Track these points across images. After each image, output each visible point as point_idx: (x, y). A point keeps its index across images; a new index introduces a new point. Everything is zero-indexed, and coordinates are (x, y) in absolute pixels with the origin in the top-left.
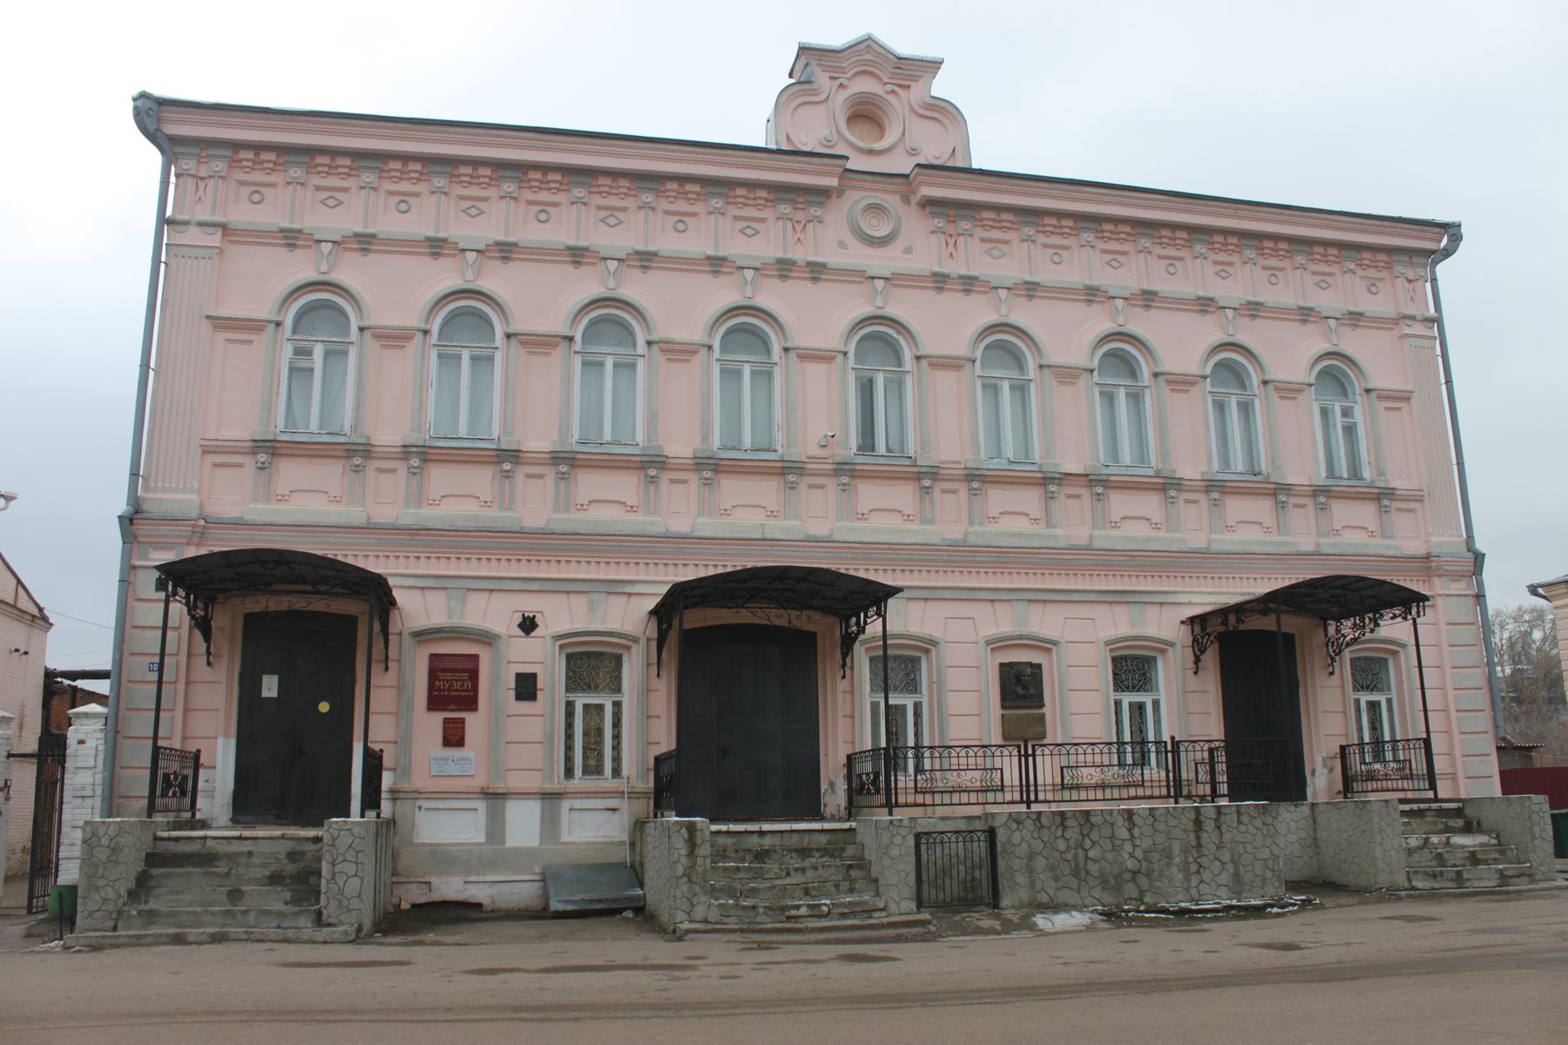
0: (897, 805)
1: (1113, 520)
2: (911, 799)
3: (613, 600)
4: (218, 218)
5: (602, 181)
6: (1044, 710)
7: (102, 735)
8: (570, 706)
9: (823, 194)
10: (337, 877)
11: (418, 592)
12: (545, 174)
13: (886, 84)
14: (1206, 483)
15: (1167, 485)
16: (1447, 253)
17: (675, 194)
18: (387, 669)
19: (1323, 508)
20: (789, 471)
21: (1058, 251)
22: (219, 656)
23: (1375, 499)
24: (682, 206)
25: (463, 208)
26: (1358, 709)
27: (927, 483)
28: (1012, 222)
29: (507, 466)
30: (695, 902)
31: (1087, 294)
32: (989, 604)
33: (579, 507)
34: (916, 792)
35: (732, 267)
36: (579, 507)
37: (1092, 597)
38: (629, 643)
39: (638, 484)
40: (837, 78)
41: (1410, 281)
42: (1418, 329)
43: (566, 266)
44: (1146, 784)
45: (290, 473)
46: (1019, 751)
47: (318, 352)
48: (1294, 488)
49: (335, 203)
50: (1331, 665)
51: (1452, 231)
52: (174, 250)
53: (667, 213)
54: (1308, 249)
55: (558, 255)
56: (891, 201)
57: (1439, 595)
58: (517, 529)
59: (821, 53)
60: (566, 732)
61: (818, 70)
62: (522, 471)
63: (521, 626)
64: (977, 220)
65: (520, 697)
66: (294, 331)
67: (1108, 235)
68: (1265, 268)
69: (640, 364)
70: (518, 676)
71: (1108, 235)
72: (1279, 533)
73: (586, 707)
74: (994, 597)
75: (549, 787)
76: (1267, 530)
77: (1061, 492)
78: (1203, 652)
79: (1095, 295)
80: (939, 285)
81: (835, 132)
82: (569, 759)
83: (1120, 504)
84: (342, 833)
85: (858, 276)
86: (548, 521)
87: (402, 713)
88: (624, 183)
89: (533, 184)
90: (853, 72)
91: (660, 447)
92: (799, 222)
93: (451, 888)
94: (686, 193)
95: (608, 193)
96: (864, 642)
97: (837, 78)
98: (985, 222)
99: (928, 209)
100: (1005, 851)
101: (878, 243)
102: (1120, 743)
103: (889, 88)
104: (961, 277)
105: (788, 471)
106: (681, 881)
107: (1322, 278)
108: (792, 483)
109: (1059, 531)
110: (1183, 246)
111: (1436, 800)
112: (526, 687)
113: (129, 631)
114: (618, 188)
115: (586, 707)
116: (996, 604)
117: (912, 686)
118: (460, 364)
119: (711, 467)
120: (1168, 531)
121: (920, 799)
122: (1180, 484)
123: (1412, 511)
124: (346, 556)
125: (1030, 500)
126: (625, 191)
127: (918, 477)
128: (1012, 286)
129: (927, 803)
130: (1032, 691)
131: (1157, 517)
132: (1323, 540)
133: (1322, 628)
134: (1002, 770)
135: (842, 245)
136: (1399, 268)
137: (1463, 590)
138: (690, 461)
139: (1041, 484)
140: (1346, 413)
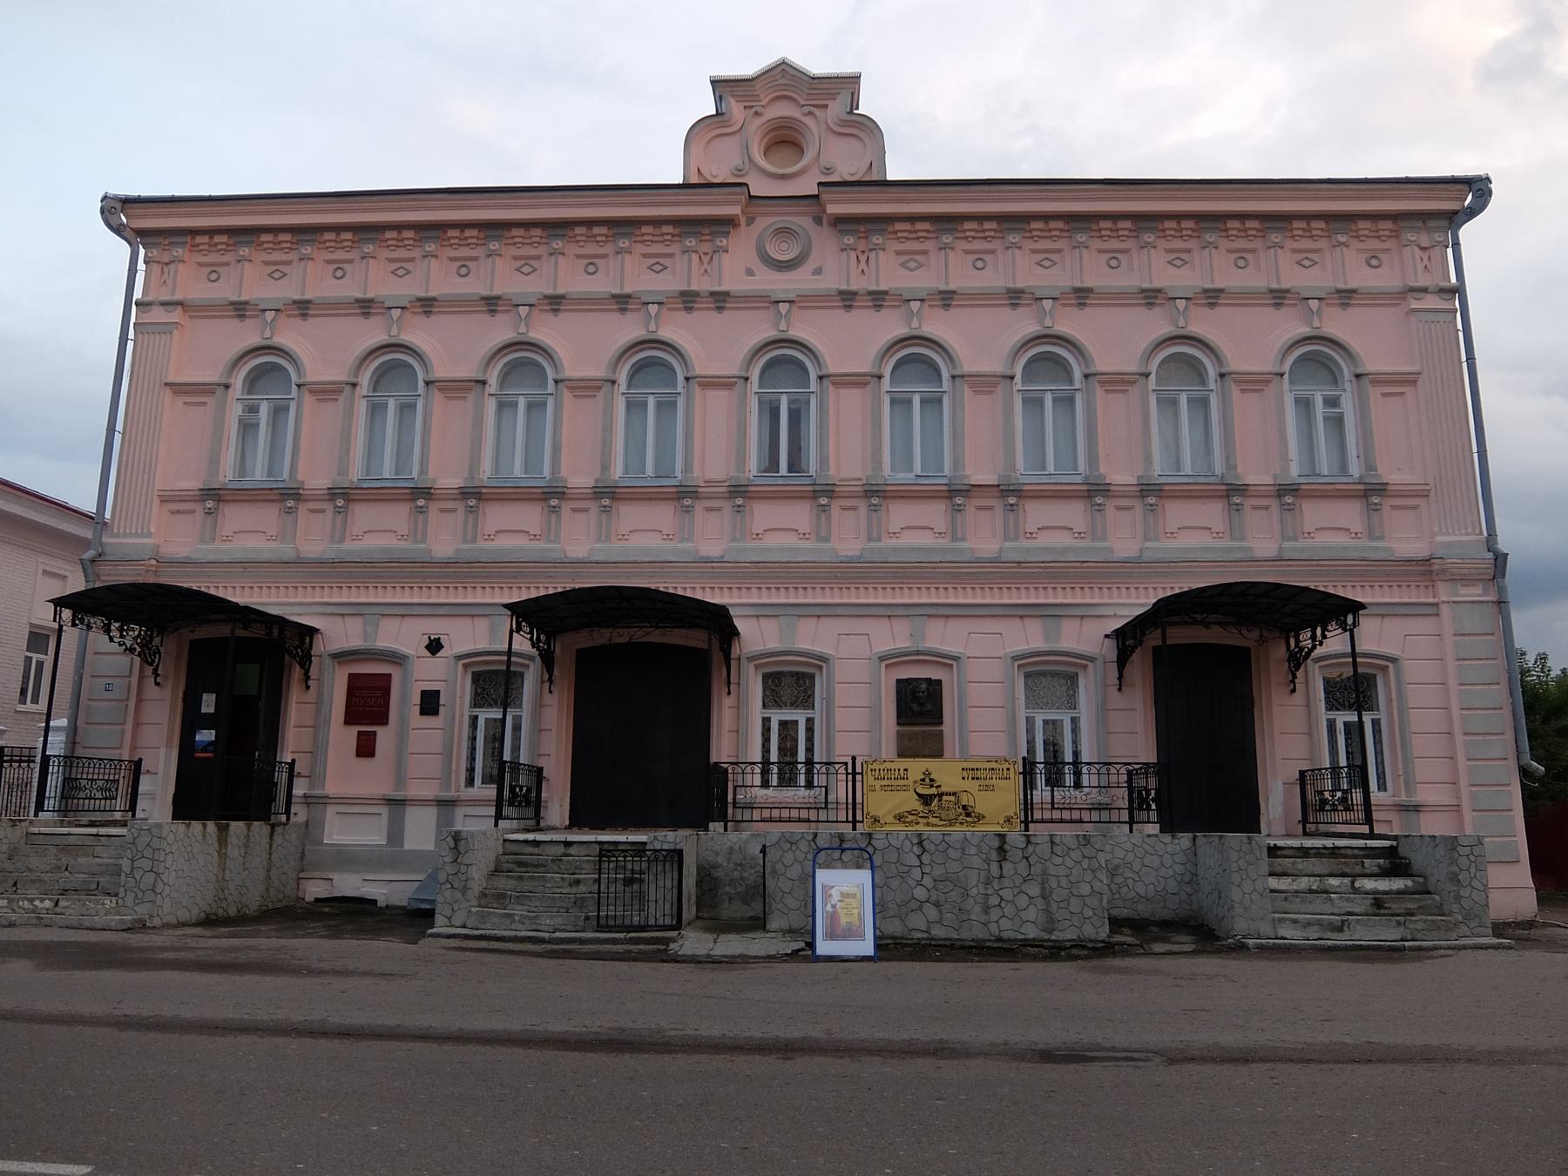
0: (1032, 822)
1: (754, 531)
2: (1047, 815)
3: (804, 621)
4: (178, 297)
5: (515, 232)
6: (942, 728)
7: (63, 746)
8: (474, 719)
9: (729, 223)
10: (135, 872)
11: (340, 619)
12: (1046, 223)
13: (803, 106)
14: (1140, 488)
15: (1094, 492)
16: (1472, 212)
17: (584, 238)
18: (308, 687)
19: (606, 510)
20: (683, 495)
21: (1115, 255)
22: (166, 678)
23: (1224, 497)
24: (591, 249)
25: (649, 264)
26: (766, 730)
27: (1012, 500)
28: (928, 231)
29: (421, 503)
30: (456, 908)
31: (1011, 298)
32: (887, 620)
33: (486, 537)
34: (1053, 808)
35: (637, 304)
36: (486, 537)
37: (999, 611)
38: (527, 662)
39: (811, 511)
40: (752, 107)
41: (1424, 249)
42: (1432, 302)
43: (1203, 308)
44: (829, 806)
45: (235, 517)
46: (846, 769)
47: (264, 409)
48: (1250, 488)
49: (660, 268)
50: (1293, 681)
51: (1477, 189)
52: (137, 327)
53: (1100, 251)
54: (1221, 225)
55: (222, 311)
56: (803, 222)
57: (1443, 602)
58: (428, 560)
59: (733, 84)
60: (813, 745)
61: (732, 101)
62: (434, 507)
63: (427, 647)
64: (1026, 231)
65: (423, 712)
66: (629, 385)
67: (1038, 233)
68: (967, 252)
69: (1078, 398)
70: (423, 692)
71: (1038, 233)
72: (1232, 539)
73: (1046, 722)
74: (889, 612)
75: (445, 795)
76: (1218, 535)
77: (970, 507)
78: (1297, 669)
79: (1019, 298)
80: (847, 303)
81: (747, 160)
82: (471, 770)
83: (1036, 514)
84: (142, 832)
85: (762, 302)
86: (1141, 550)
87: (318, 727)
88: (537, 232)
89: (452, 241)
90: (770, 97)
91: (1237, 477)
92: (706, 254)
93: (349, 884)
94: (595, 236)
95: (539, 243)
96: (1319, 659)
97: (752, 107)
98: (899, 235)
99: (840, 227)
100: (774, 871)
101: (786, 267)
102: (766, 763)
103: (806, 109)
104: (870, 293)
105: (684, 495)
106: (444, 887)
107: (1305, 255)
108: (687, 507)
109: (965, 545)
110: (1320, 236)
111: (1372, 836)
112: (430, 703)
113: (89, 656)
114: (531, 237)
115: (1046, 722)
116: (893, 620)
117: (806, 701)
118: (910, 410)
119: (608, 495)
120: (1093, 540)
121: (1057, 815)
122: (1108, 490)
123: (1415, 508)
124: (676, 588)
125: (934, 514)
126: (538, 239)
127: (815, 495)
128: (926, 297)
129: (812, 819)
130: (929, 707)
131: (1080, 526)
132: (1287, 545)
133: (1284, 640)
134: (826, 787)
135: (750, 272)
136: (1411, 236)
137: (1480, 595)
138: (196, 493)
139: (947, 498)
140: (1332, 402)
